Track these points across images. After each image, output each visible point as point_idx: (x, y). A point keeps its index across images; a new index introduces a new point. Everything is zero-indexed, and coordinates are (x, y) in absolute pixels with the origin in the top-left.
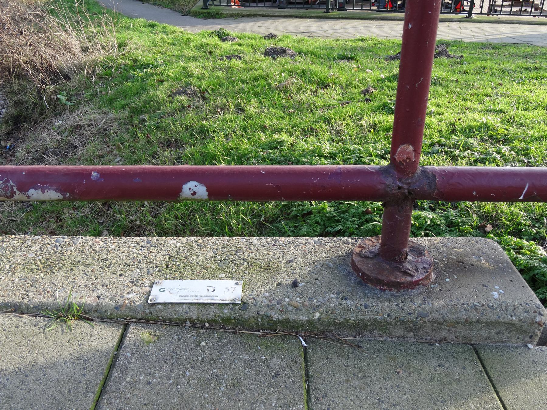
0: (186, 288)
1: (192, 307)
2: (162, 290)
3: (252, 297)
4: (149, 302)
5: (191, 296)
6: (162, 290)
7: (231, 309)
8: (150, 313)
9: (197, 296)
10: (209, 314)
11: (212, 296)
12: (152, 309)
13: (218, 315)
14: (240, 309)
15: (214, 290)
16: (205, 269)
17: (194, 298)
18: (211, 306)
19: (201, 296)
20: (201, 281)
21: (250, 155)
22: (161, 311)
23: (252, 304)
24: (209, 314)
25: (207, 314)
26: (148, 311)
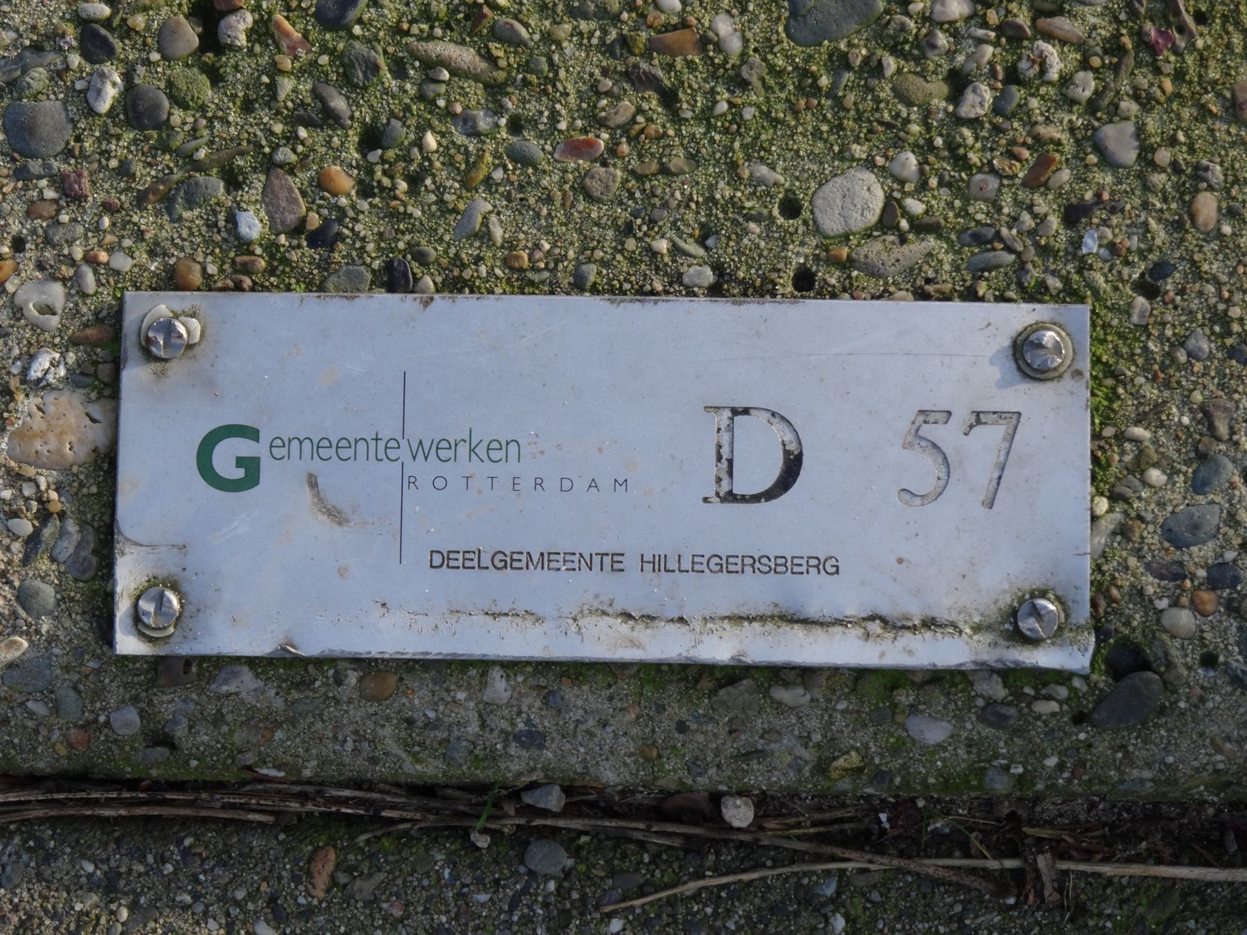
0: (483, 433)
1: (578, 699)
2: (225, 458)
3: (1201, 554)
4: (128, 644)
5: (546, 559)
6: (225, 458)
7: (991, 713)
8: (163, 739)
9: (614, 562)
10: (761, 754)
11: (781, 565)
12: (170, 704)
13: (854, 759)
14: (1079, 719)
15: (792, 467)
16: (650, 82)
17: (593, 584)
18: (780, 694)
19: (658, 564)
20: (632, 312)
21: (1042, 862)
22: (267, 722)
23: (1209, 661)
24: (761, 754)
25: (747, 756)
26: (128, 720)
